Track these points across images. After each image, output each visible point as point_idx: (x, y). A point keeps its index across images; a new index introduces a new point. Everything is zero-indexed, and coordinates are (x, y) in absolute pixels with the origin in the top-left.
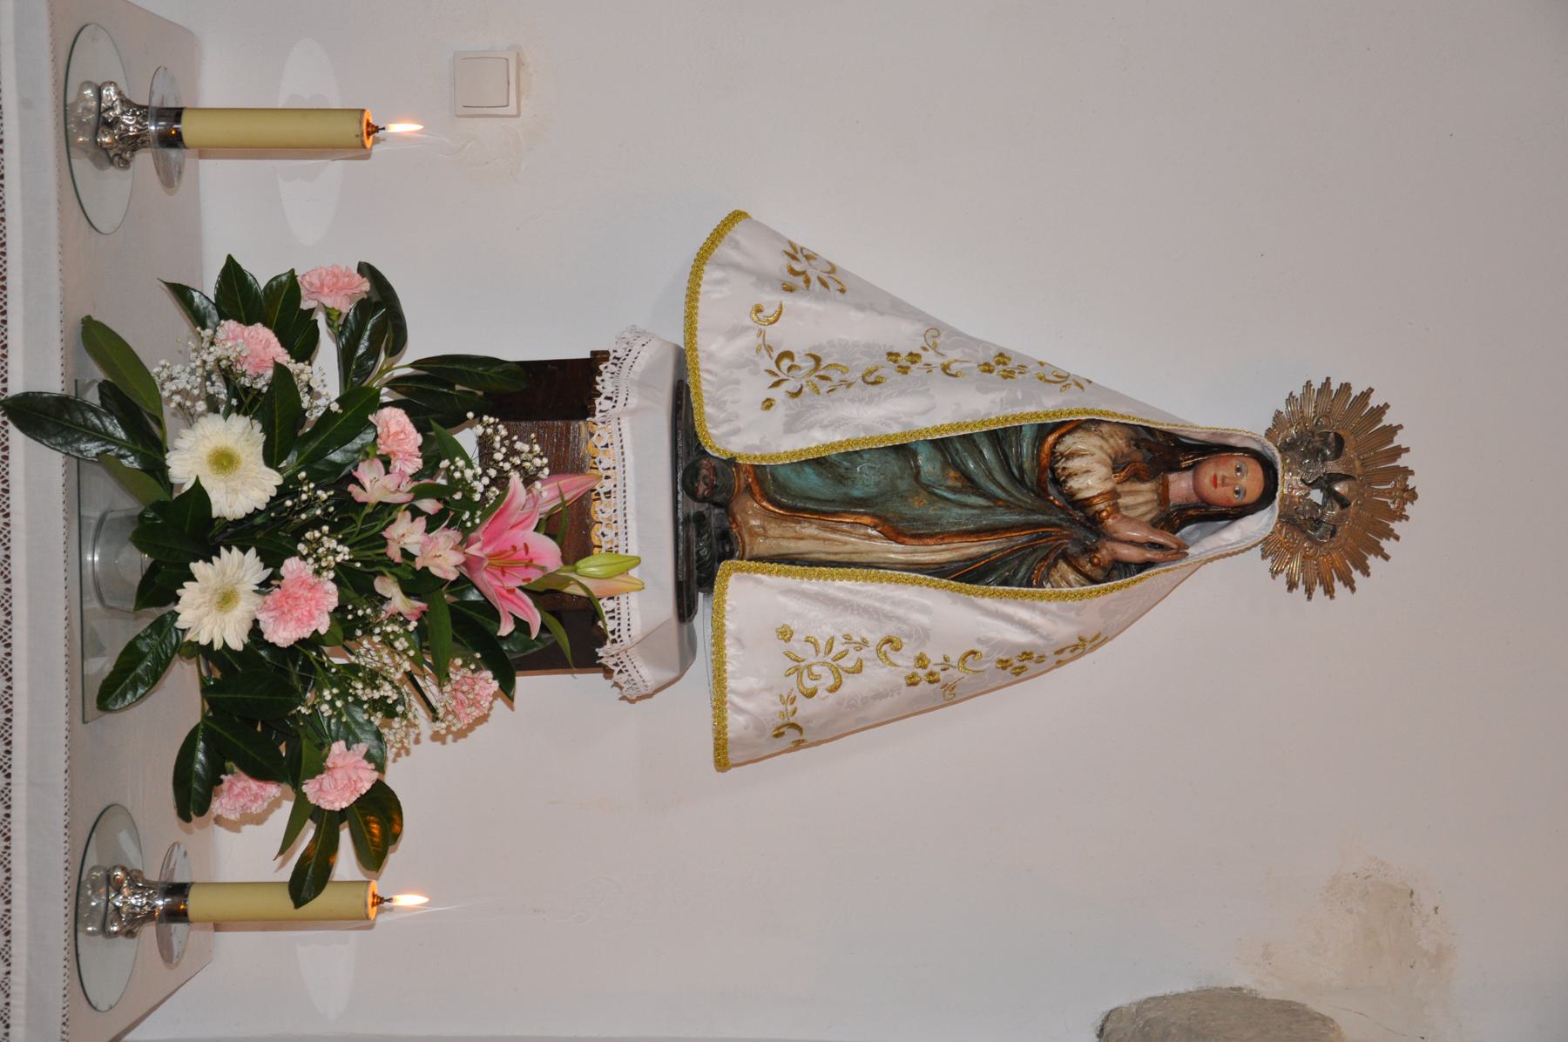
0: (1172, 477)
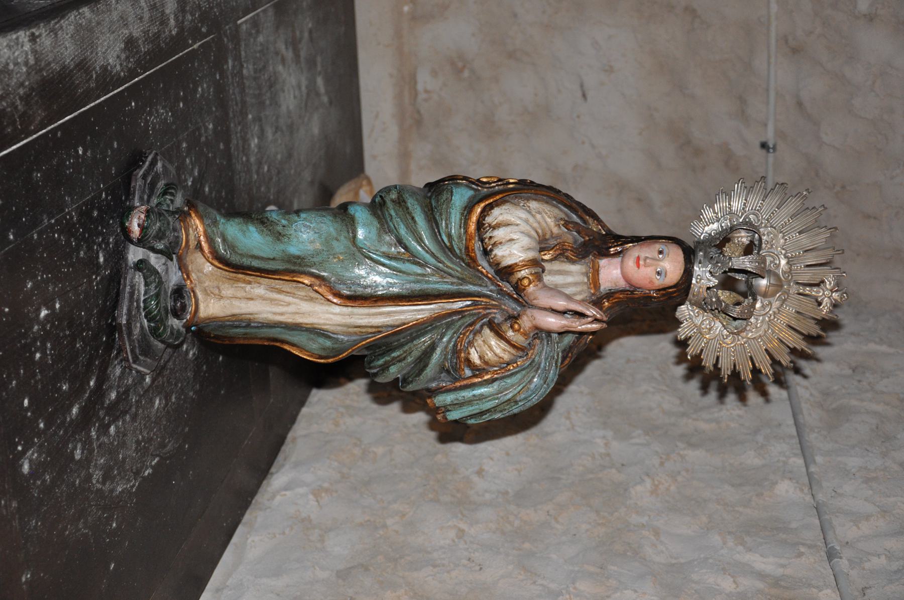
0: (603, 262)
